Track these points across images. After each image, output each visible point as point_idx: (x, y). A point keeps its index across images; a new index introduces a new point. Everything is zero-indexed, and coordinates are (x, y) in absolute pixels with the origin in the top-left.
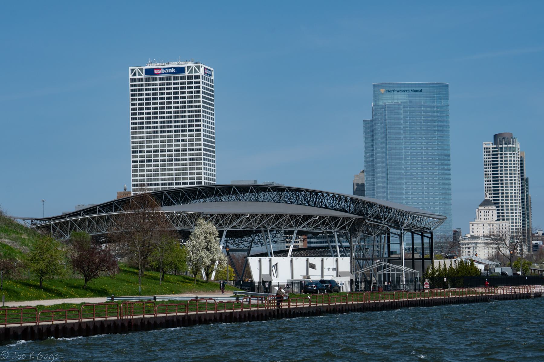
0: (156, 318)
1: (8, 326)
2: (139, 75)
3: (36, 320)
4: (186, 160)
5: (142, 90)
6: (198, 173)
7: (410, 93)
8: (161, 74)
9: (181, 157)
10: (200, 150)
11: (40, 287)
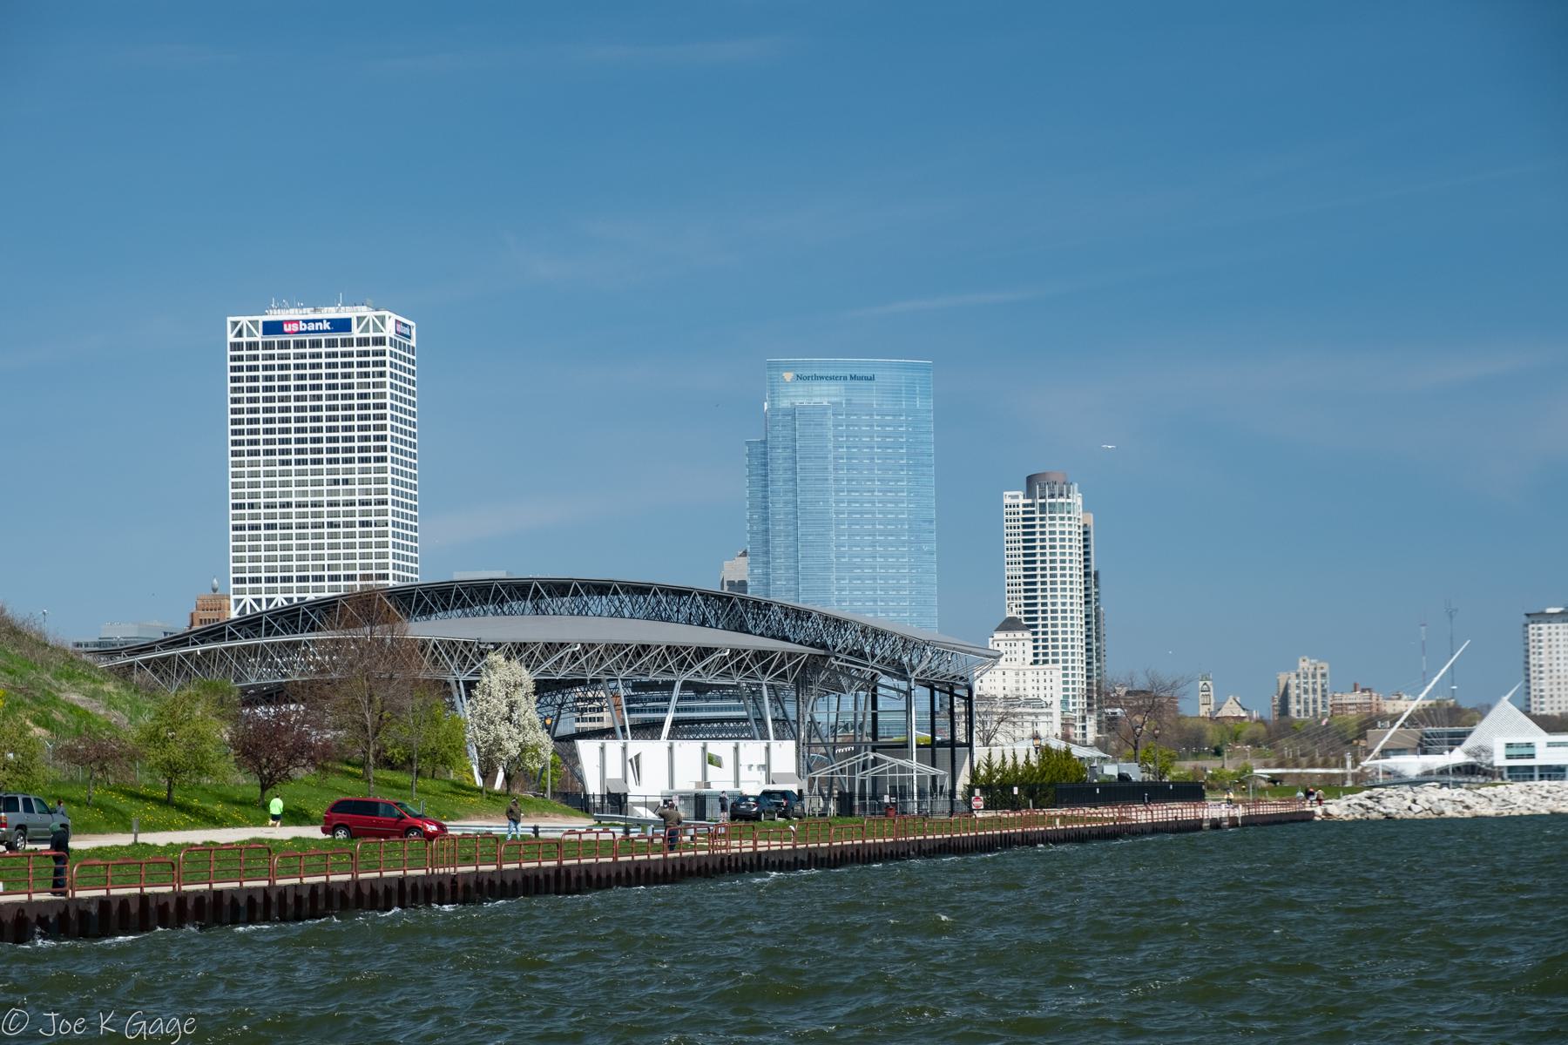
0: (500, 871)
1: (147, 890)
2: (250, 334)
3: (498, 860)
4: (352, 525)
5: (256, 368)
6: (379, 556)
7: (849, 382)
8: (299, 332)
9: (341, 519)
10: (384, 502)
11: (167, 803)
